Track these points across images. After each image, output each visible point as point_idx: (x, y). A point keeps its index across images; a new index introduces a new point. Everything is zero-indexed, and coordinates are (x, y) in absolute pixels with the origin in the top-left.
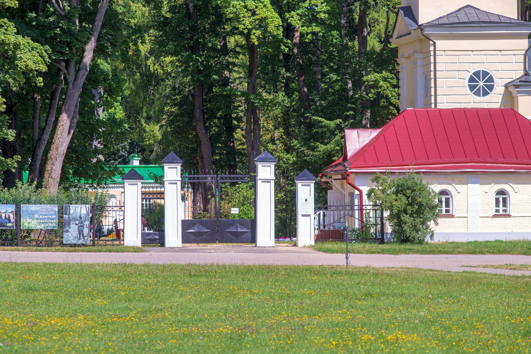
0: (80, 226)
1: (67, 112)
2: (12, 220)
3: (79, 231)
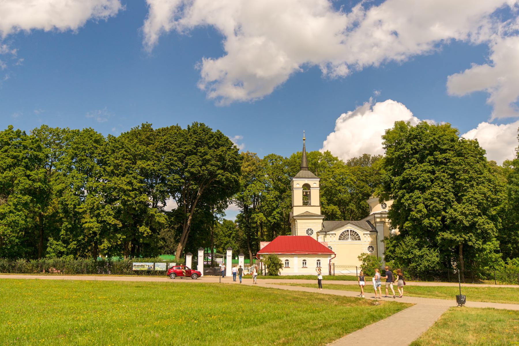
2: (153, 267)
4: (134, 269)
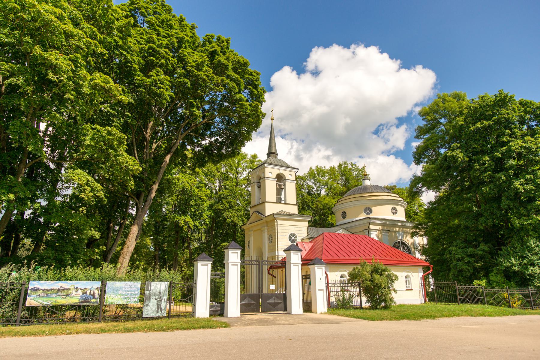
0: (159, 301)
1: (137, 224)
2: (97, 296)
3: (158, 305)
4: (31, 301)
